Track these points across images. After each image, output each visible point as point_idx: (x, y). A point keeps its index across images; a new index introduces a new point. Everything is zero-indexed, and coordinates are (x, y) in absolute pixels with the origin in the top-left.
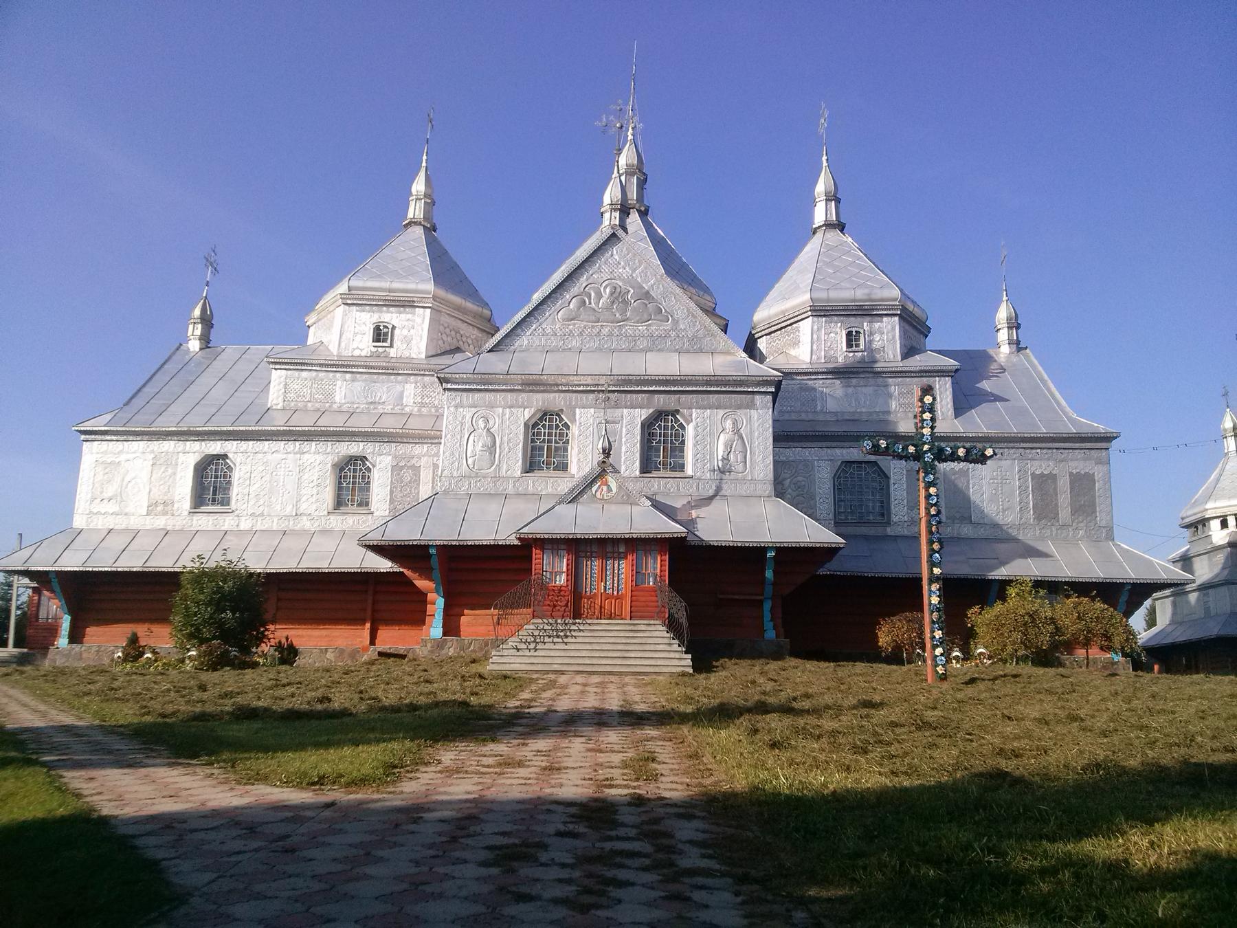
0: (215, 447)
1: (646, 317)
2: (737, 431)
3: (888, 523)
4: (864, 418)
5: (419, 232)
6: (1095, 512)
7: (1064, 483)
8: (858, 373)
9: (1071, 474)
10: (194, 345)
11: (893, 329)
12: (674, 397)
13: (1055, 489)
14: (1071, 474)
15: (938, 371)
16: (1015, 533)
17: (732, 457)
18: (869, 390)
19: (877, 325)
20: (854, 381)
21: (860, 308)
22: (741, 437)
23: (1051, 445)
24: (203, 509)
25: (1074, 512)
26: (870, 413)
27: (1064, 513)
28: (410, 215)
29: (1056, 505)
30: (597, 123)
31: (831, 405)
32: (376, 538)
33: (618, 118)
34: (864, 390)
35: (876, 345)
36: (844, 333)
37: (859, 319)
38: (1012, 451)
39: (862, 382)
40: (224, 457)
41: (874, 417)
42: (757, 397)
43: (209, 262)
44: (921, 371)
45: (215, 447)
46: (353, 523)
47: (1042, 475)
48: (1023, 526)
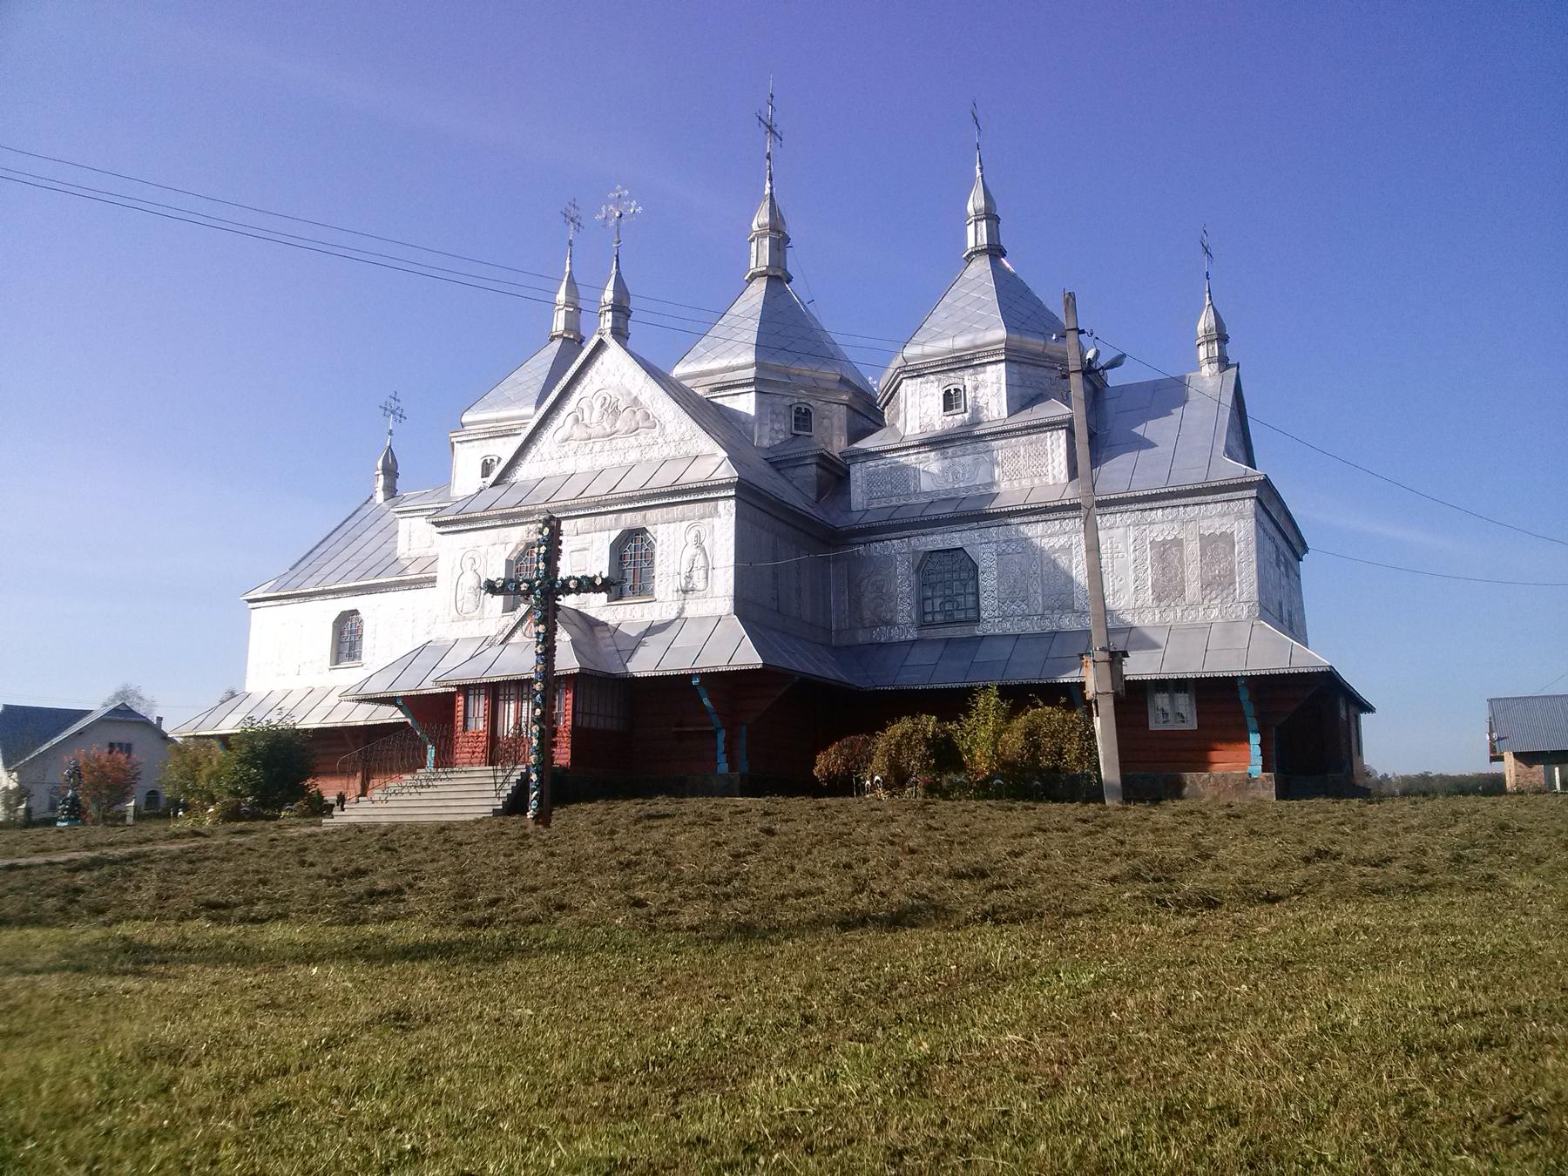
0: (347, 603)
1: (634, 425)
2: (699, 544)
3: (977, 620)
4: (964, 495)
5: (982, 266)
6: (1233, 583)
7: (1192, 548)
8: (953, 440)
9: (1202, 537)
10: (380, 497)
11: (998, 381)
12: (638, 516)
13: (1181, 558)
14: (1202, 537)
15: (1048, 425)
16: (1129, 618)
17: (695, 574)
18: (968, 459)
19: (980, 377)
20: (950, 451)
21: (960, 359)
22: (704, 550)
23: (1175, 502)
24: (343, 665)
25: (1206, 585)
26: (968, 488)
27: (1193, 589)
28: (971, 244)
29: (1182, 579)
30: (598, 217)
31: (926, 484)
32: (378, 687)
33: (617, 206)
34: (963, 460)
35: (982, 402)
36: (942, 393)
37: (960, 373)
38: (1125, 516)
39: (959, 451)
40: (355, 612)
41: (973, 493)
42: (721, 503)
43: (388, 410)
44: (1027, 428)
45: (347, 603)
46: (349, 677)
47: (1164, 543)
48: (1139, 611)
